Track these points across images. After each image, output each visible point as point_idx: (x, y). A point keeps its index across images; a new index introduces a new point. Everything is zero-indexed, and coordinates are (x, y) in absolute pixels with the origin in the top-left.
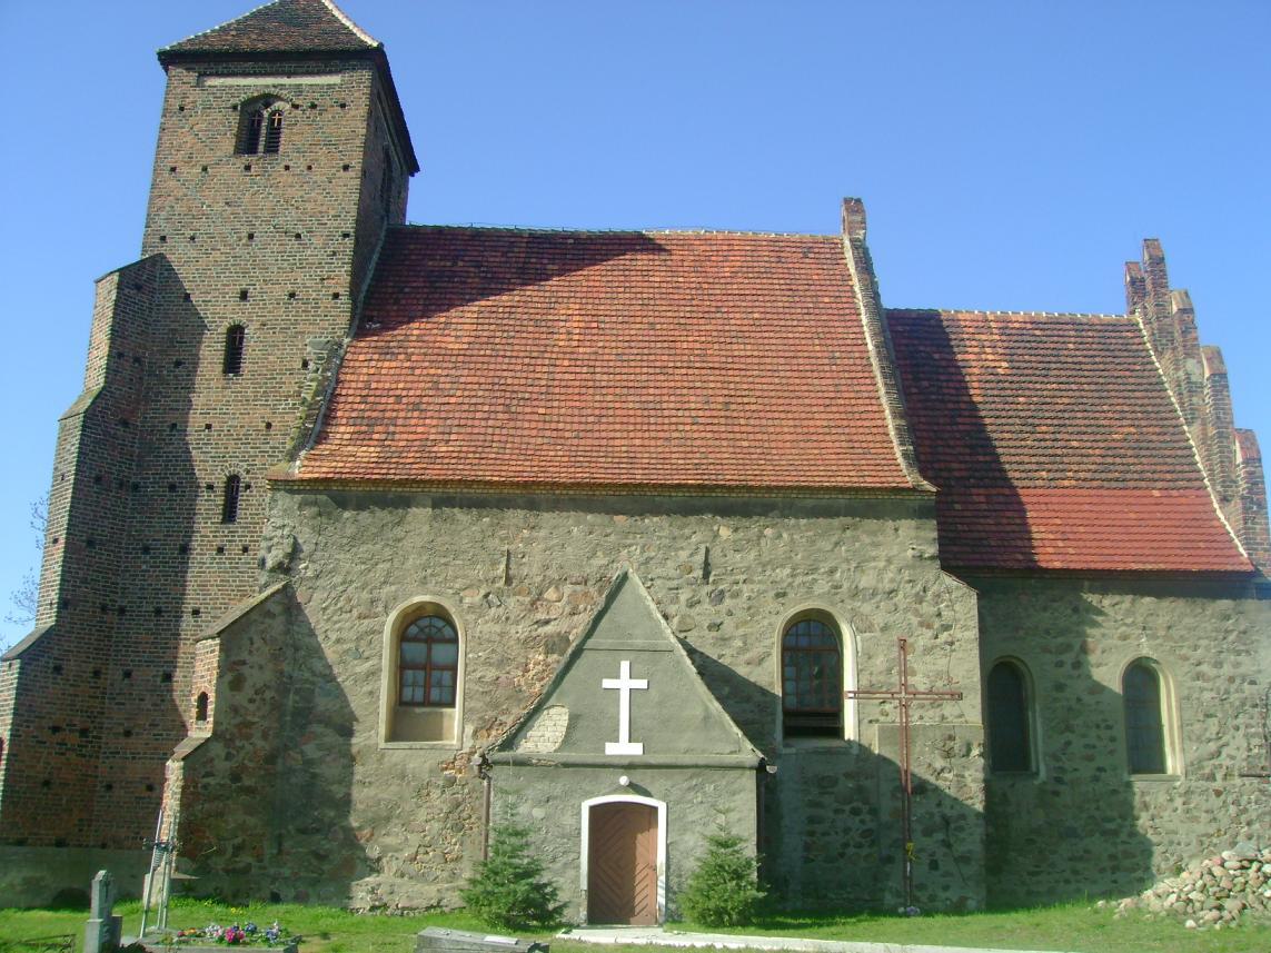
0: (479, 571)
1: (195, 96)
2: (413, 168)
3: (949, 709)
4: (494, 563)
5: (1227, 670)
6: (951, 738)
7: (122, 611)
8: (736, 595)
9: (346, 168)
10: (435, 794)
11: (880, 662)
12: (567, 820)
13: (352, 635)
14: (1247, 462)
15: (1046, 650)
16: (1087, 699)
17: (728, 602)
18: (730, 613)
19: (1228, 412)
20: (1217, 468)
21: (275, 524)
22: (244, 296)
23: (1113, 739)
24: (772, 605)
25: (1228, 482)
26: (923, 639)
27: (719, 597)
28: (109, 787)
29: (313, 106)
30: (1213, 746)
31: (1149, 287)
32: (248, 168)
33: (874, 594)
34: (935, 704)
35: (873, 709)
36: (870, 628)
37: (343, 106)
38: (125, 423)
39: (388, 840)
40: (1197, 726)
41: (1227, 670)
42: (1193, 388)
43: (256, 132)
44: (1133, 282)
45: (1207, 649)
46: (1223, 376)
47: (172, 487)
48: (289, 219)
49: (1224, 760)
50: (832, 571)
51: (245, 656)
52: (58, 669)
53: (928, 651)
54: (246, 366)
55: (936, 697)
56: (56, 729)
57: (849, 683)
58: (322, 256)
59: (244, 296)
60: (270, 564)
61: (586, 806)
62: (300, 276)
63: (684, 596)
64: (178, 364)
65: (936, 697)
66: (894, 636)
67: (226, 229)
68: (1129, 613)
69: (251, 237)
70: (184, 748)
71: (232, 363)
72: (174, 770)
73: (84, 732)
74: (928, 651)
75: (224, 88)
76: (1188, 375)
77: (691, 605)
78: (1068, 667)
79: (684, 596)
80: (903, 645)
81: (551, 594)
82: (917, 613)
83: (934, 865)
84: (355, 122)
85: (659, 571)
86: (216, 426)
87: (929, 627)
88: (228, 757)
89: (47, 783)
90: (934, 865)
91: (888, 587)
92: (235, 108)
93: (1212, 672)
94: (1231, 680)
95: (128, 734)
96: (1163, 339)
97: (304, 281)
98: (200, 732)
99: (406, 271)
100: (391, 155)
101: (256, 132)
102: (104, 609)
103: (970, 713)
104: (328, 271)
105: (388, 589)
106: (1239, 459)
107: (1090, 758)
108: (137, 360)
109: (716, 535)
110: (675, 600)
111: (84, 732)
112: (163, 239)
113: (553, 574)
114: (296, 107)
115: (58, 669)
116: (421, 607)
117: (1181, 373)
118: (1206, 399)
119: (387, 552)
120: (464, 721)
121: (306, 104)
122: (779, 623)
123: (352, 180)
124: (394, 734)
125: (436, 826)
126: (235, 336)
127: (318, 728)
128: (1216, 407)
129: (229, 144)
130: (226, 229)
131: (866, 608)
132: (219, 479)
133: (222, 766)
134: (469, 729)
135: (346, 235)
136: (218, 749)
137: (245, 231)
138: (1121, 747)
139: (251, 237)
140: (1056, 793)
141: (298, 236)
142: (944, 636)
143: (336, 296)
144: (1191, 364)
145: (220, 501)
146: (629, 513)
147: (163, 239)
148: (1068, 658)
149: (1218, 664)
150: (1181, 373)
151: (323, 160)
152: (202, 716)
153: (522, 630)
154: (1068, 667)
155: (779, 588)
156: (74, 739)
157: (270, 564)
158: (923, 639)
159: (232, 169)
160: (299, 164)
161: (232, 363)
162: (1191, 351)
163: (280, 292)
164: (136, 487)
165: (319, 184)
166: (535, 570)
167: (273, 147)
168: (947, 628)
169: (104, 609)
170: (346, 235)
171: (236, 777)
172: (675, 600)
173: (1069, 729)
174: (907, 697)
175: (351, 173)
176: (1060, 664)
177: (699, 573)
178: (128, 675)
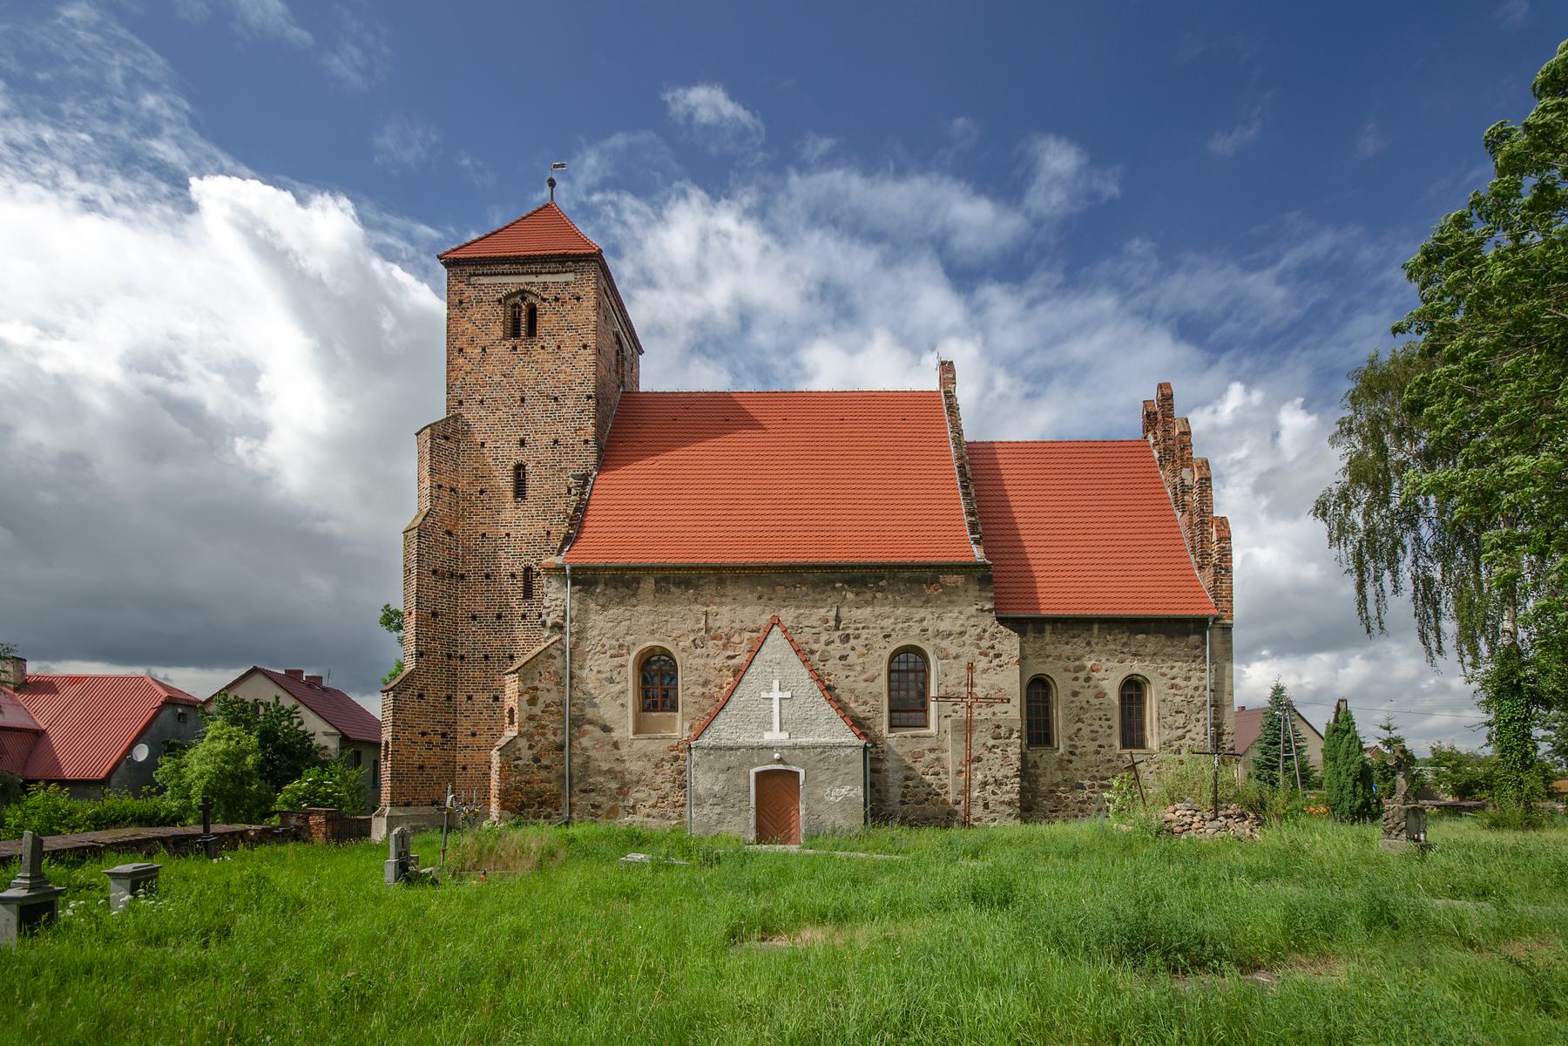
0: (690, 624)
1: (470, 292)
2: (640, 351)
3: (998, 708)
4: (698, 621)
5: (1194, 682)
6: (998, 727)
7: (462, 657)
8: (857, 637)
9: (585, 347)
10: (667, 766)
11: (952, 679)
12: (742, 781)
13: (607, 668)
14: (1220, 540)
15: (1066, 670)
16: (1094, 701)
17: (852, 642)
18: (853, 649)
19: (1210, 506)
20: (1198, 546)
21: (557, 598)
22: (522, 443)
23: (1110, 727)
24: (883, 643)
25: (1205, 555)
26: (982, 663)
27: (846, 638)
28: (464, 768)
29: (557, 299)
30: (1180, 732)
31: (1160, 417)
32: (515, 348)
33: (950, 635)
34: (990, 705)
35: (948, 707)
36: (946, 657)
37: (578, 299)
38: (450, 533)
39: (638, 795)
40: (1170, 719)
41: (1194, 682)
42: (1186, 489)
43: (522, 322)
44: (1148, 415)
45: (1181, 668)
46: (1209, 479)
47: (487, 576)
48: (547, 386)
49: (1187, 741)
50: (922, 620)
51: (536, 683)
52: (421, 696)
53: (985, 671)
54: (529, 492)
55: (989, 701)
56: (424, 734)
57: (933, 692)
58: (573, 413)
59: (522, 443)
60: (549, 624)
61: (753, 771)
62: (560, 427)
63: (824, 637)
64: (482, 492)
65: (989, 701)
66: (964, 661)
67: (505, 395)
68: (1124, 645)
69: (523, 400)
70: (502, 742)
71: (520, 490)
72: (495, 756)
73: (444, 735)
74: (985, 671)
75: (488, 286)
76: (1182, 480)
77: (827, 644)
78: (1081, 680)
79: (824, 637)
80: (971, 668)
81: (736, 639)
82: (978, 647)
83: (986, 806)
84: (586, 312)
85: (806, 623)
86: (513, 534)
87: (986, 655)
88: (531, 747)
89: (421, 767)
90: (986, 806)
91: (959, 629)
92: (500, 301)
93: (1183, 684)
94: (1196, 689)
95: (474, 735)
96: (1167, 453)
97: (564, 431)
98: (510, 733)
99: (629, 422)
100: (621, 345)
101: (522, 322)
102: (449, 656)
103: (1013, 712)
104: (577, 426)
105: (628, 638)
106: (1215, 538)
107: (1094, 740)
108: (453, 490)
109: (845, 597)
110: (817, 641)
111: (444, 735)
112: (461, 402)
113: (737, 625)
114: (544, 300)
115: (421, 696)
116: (652, 649)
117: (1177, 480)
118: (1193, 499)
119: (628, 614)
120: (683, 720)
121: (551, 298)
122: (886, 654)
123: (588, 356)
124: (637, 731)
125: (669, 785)
126: (520, 470)
127: (587, 727)
128: (1201, 502)
129: (498, 331)
130: (505, 395)
131: (945, 644)
132: (518, 569)
133: (527, 754)
134: (687, 725)
135: (589, 397)
136: (523, 743)
137: (518, 395)
138: (1117, 731)
139: (523, 400)
140: (1070, 762)
141: (556, 399)
142: (996, 662)
143: (586, 442)
144: (1185, 473)
145: (520, 584)
146: (598, 436)
147: (461, 402)
148: (1082, 675)
149: (1188, 679)
150: (1177, 480)
151: (568, 342)
152: (512, 722)
153: (719, 661)
154: (1081, 680)
155: (886, 632)
156: (437, 739)
157: (549, 624)
158: (982, 663)
159: (502, 351)
160: (551, 344)
161: (520, 490)
162: (1187, 462)
163: (547, 440)
164: (462, 577)
165: (567, 362)
166: (724, 623)
167: (532, 331)
168: (998, 656)
169: (449, 656)
170: (589, 397)
171: (536, 760)
172: (817, 641)
173: (1080, 720)
174: (972, 701)
175: (589, 351)
176: (1076, 679)
177: (832, 623)
178: (470, 698)
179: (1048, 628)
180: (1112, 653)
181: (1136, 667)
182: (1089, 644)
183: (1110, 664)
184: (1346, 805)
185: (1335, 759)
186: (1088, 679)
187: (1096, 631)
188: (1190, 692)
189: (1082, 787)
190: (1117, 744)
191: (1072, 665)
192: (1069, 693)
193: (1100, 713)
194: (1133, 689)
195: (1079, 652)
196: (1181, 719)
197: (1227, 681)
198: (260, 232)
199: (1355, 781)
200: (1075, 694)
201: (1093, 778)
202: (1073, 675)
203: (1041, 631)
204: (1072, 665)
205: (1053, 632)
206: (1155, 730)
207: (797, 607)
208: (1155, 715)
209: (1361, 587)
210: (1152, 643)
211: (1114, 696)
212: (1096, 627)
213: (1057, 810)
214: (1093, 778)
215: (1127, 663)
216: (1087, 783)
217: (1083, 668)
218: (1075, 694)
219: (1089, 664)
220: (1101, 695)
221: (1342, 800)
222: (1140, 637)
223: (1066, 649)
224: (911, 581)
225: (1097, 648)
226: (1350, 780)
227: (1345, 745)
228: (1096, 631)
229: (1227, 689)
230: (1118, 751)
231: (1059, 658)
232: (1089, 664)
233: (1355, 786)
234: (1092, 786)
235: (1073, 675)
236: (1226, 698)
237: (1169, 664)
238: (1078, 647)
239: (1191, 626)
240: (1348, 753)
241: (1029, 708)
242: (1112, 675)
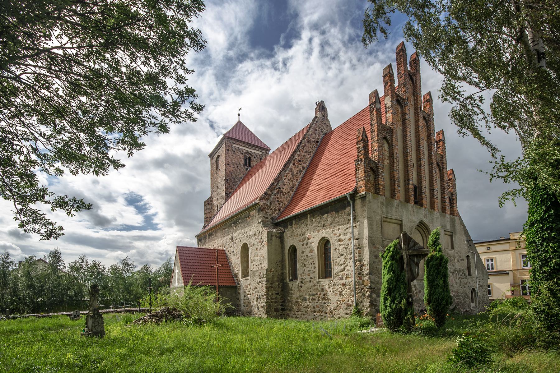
5: (349, 236)
16: (309, 255)
30: (342, 267)
40: (338, 259)
148: (305, 242)
149: (346, 234)
176: (303, 245)
180: (315, 228)
181: (324, 233)
188: (346, 242)
189: (305, 299)
191: (302, 238)
194: (325, 244)
196: (343, 259)
198: (410, 300)
201: (309, 295)
202: (301, 243)
203: (291, 224)
204: (302, 238)
207: (128, 321)
209: (476, 134)
210: (328, 218)
213: (300, 315)
214: (309, 295)
215: (321, 232)
216: (308, 297)
219: (307, 236)
222: (325, 216)
224: (245, 217)
237: (337, 227)
238: (303, 228)
239: (119, 228)
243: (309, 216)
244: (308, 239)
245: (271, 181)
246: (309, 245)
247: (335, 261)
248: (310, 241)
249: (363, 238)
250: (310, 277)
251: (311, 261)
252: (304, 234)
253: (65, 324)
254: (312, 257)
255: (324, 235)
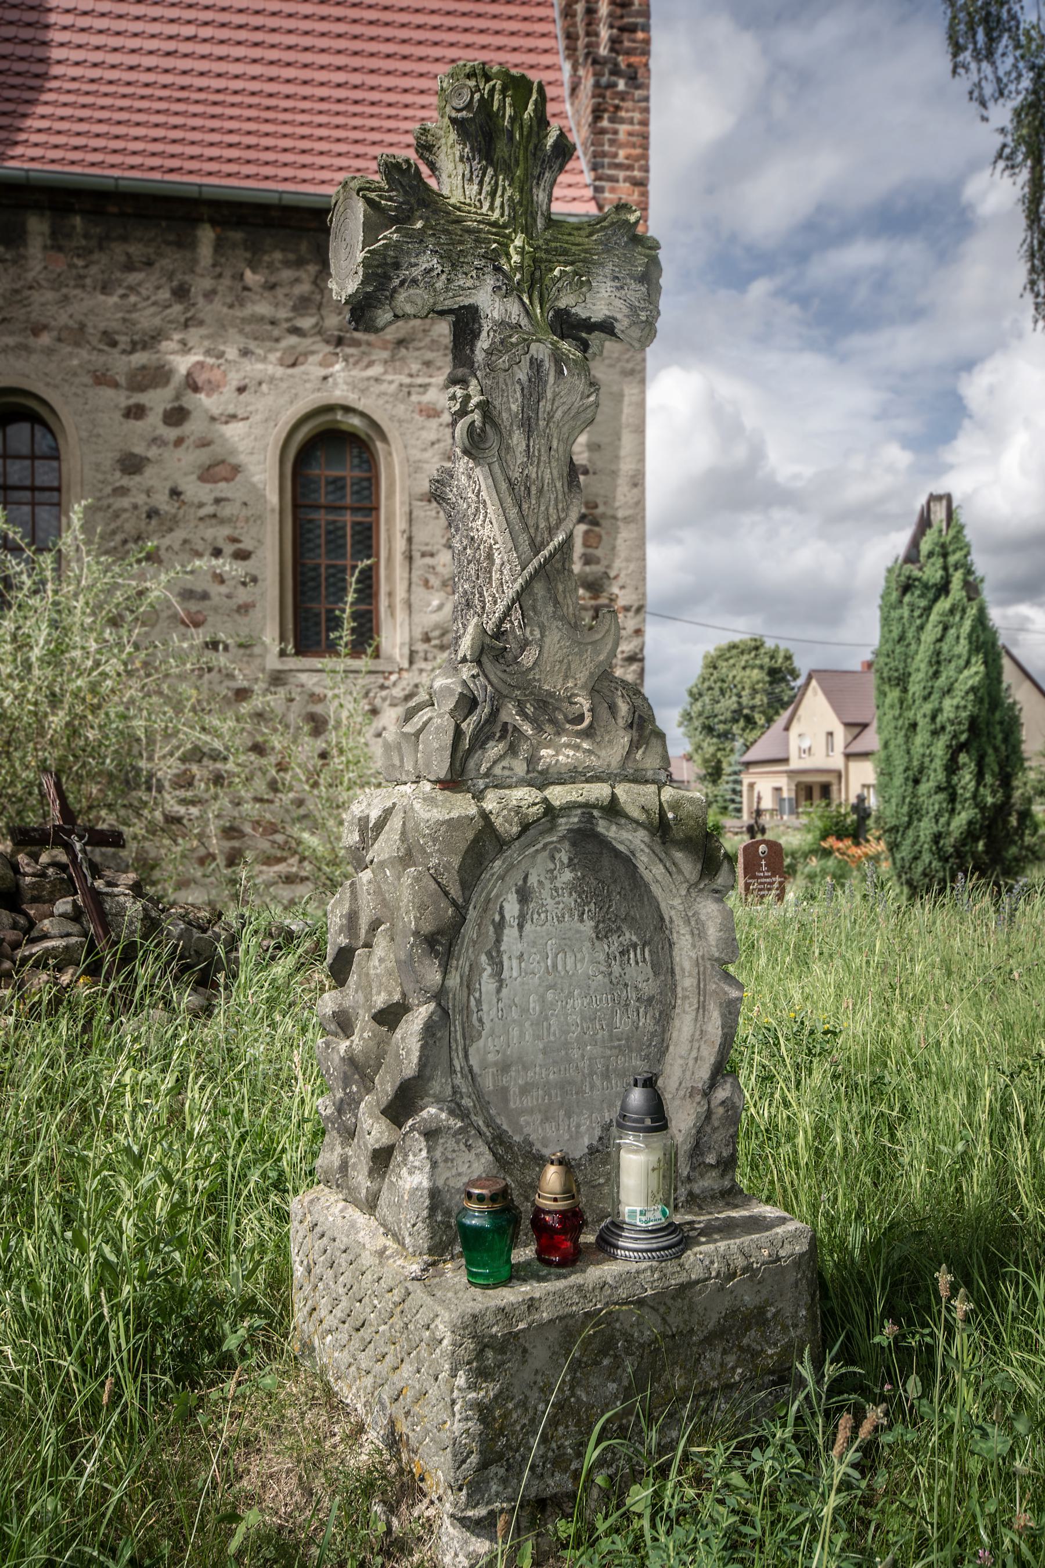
15: (102, 379)
16: (195, 490)
78: (154, 420)
148: (158, 400)
154: (154, 420)
176: (136, 412)
179: (37, 226)
180: (264, 332)
182: (181, 293)
183: (254, 368)
184: (926, 828)
185: (901, 681)
186: (177, 416)
187: (205, 251)
190: (270, 637)
191: (122, 364)
192: (108, 458)
193: (219, 533)
195: (147, 319)
197: (627, 440)
199: (955, 751)
200: (132, 464)
202: (123, 399)
205: (57, 241)
206: (400, 593)
208: (400, 545)
211: (264, 475)
212: (206, 235)
215: (312, 369)
217: (159, 375)
218: (132, 464)
220: (220, 469)
221: (915, 813)
223: (106, 308)
225: (206, 310)
226: (939, 748)
227: (930, 634)
228: (205, 251)
229: (626, 467)
230: (273, 662)
231: (77, 335)
232: (183, 365)
233: (952, 767)
234: (185, 781)
235: (123, 399)
236: (623, 494)
238: (146, 299)
240: (937, 661)
241: (370, 538)
242: (260, 404)
243: (206, 235)
244: (192, 385)
245: (654, 128)
246: (193, 427)
247: (419, 562)
248: (207, 402)
249: (614, 474)
250: (200, 636)
251: (219, 533)
252: (150, 340)
253: (346, 908)
254: (227, 511)
255: (340, 393)
